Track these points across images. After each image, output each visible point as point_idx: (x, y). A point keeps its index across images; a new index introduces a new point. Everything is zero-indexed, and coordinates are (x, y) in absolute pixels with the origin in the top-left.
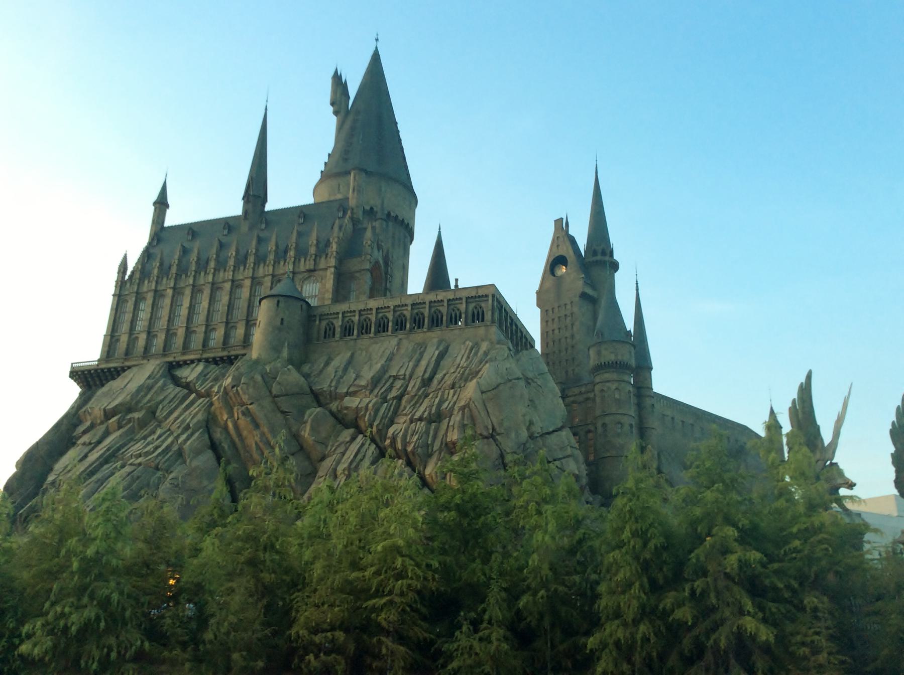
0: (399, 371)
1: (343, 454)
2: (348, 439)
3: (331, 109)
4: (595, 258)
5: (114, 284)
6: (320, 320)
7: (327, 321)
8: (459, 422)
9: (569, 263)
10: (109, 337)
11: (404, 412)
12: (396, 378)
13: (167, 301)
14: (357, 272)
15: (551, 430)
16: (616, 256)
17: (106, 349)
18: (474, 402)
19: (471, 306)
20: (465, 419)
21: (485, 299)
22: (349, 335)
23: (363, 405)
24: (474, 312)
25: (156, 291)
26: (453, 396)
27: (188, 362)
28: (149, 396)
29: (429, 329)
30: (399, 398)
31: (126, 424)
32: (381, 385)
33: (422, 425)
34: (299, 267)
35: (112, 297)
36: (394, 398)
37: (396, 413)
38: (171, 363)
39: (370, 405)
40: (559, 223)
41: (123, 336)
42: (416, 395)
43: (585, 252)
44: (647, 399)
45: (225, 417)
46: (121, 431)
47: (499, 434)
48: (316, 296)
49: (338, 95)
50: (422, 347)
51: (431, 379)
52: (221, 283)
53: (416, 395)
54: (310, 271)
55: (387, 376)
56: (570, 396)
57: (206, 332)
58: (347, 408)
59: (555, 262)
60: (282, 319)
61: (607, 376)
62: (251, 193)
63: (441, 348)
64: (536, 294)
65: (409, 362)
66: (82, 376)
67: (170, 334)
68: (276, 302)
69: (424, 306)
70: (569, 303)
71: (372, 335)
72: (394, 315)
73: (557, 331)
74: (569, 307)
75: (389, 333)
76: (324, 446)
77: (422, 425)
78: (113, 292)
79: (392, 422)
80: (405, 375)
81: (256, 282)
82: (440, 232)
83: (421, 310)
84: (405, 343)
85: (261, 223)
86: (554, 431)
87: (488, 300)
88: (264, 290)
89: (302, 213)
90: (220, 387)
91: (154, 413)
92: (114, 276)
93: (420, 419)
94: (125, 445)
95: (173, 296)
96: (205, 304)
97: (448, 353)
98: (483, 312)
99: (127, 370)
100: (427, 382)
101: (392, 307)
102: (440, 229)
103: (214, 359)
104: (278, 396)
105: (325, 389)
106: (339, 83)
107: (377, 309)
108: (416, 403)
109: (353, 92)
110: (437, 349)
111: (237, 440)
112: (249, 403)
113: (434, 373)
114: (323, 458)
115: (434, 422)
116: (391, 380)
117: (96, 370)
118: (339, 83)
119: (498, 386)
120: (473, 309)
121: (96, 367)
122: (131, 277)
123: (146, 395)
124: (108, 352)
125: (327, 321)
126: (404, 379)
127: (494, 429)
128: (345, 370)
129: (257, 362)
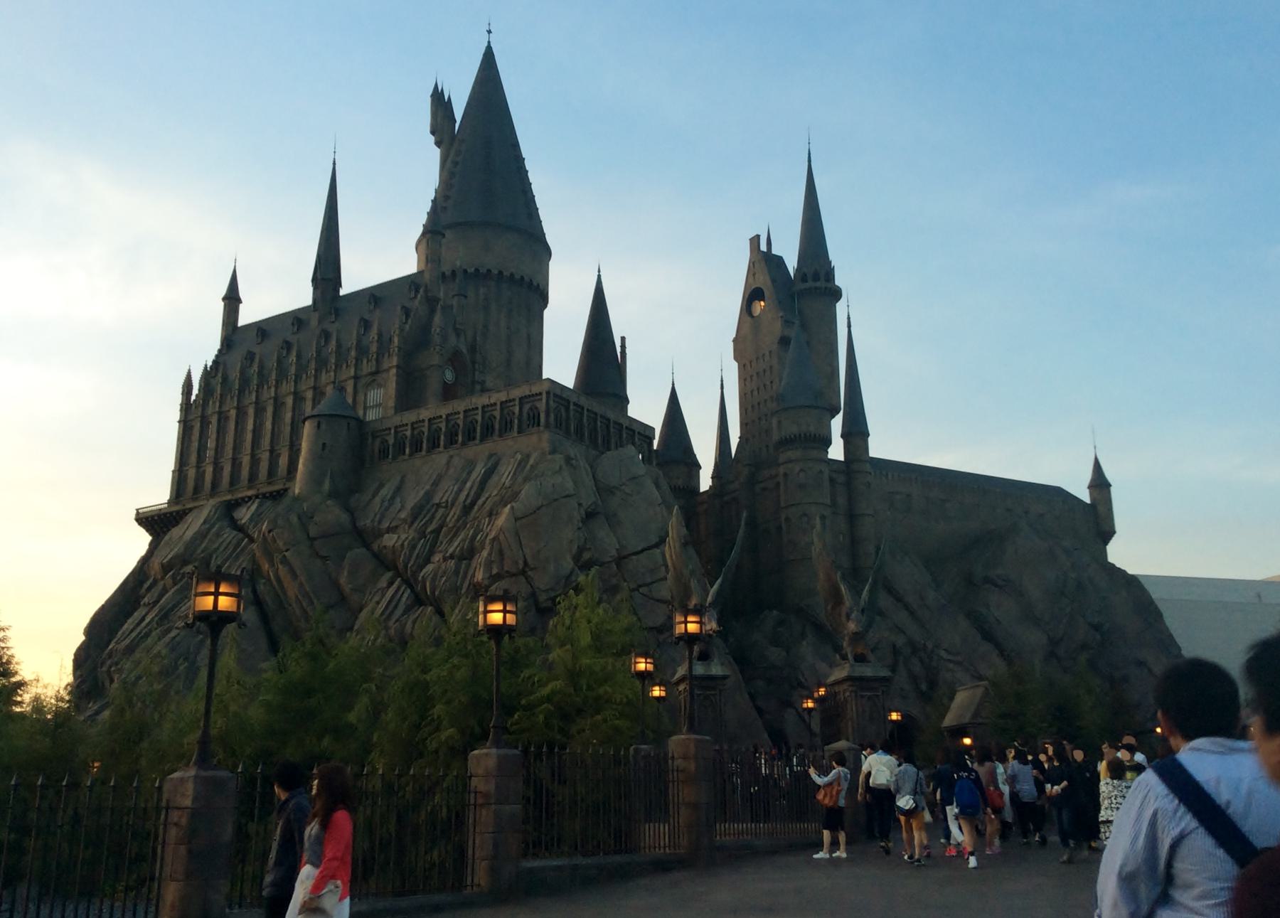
0: (442, 498)
1: (378, 603)
3: (432, 139)
4: (818, 284)
5: (179, 407)
8: (487, 558)
9: (766, 298)
11: (440, 549)
12: (438, 505)
15: (640, 549)
16: (839, 281)
17: (175, 488)
18: (504, 533)
19: (527, 407)
20: (493, 555)
21: (539, 397)
25: (220, 413)
27: (246, 499)
28: (203, 545)
29: (482, 440)
30: (437, 531)
31: (181, 580)
32: (422, 516)
33: (452, 563)
34: (362, 370)
35: (178, 424)
36: (432, 532)
37: (431, 552)
38: (229, 501)
39: (406, 543)
40: (755, 241)
41: (190, 470)
43: (795, 275)
45: (267, 566)
46: (176, 588)
47: (532, 569)
48: (380, 404)
49: (439, 119)
50: (471, 465)
51: (473, 503)
55: (431, 504)
58: (385, 547)
59: (752, 295)
61: (791, 454)
62: (319, 277)
65: (454, 485)
67: (255, 461)
68: (316, 424)
69: (476, 412)
71: (424, 453)
72: (447, 426)
73: (755, 393)
74: (767, 358)
75: (441, 449)
78: (178, 418)
79: (428, 561)
80: (447, 501)
81: (299, 399)
83: (511, 408)
84: (456, 461)
85: (331, 314)
86: (642, 551)
87: (541, 399)
90: (260, 532)
92: (178, 399)
93: (452, 557)
94: (179, 603)
95: (237, 416)
99: (188, 513)
100: (467, 509)
101: (444, 416)
102: (599, 271)
103: (271, 493)
104: (315, 539)
105: (368, 525)
107: (430, 420)
109: (459, 115)
110: (485, 465)
111: (279, 592)
112: (284, 549)
113: (478, 496)
114: (361, 610)
115: (465, 559)
118: (440, 102)
119: (538, 509)
121: (166, 511)
123: (202, 542)
126: (446, 507)
127: (526, 563)
128: (393, 498)
129: (297, 499)
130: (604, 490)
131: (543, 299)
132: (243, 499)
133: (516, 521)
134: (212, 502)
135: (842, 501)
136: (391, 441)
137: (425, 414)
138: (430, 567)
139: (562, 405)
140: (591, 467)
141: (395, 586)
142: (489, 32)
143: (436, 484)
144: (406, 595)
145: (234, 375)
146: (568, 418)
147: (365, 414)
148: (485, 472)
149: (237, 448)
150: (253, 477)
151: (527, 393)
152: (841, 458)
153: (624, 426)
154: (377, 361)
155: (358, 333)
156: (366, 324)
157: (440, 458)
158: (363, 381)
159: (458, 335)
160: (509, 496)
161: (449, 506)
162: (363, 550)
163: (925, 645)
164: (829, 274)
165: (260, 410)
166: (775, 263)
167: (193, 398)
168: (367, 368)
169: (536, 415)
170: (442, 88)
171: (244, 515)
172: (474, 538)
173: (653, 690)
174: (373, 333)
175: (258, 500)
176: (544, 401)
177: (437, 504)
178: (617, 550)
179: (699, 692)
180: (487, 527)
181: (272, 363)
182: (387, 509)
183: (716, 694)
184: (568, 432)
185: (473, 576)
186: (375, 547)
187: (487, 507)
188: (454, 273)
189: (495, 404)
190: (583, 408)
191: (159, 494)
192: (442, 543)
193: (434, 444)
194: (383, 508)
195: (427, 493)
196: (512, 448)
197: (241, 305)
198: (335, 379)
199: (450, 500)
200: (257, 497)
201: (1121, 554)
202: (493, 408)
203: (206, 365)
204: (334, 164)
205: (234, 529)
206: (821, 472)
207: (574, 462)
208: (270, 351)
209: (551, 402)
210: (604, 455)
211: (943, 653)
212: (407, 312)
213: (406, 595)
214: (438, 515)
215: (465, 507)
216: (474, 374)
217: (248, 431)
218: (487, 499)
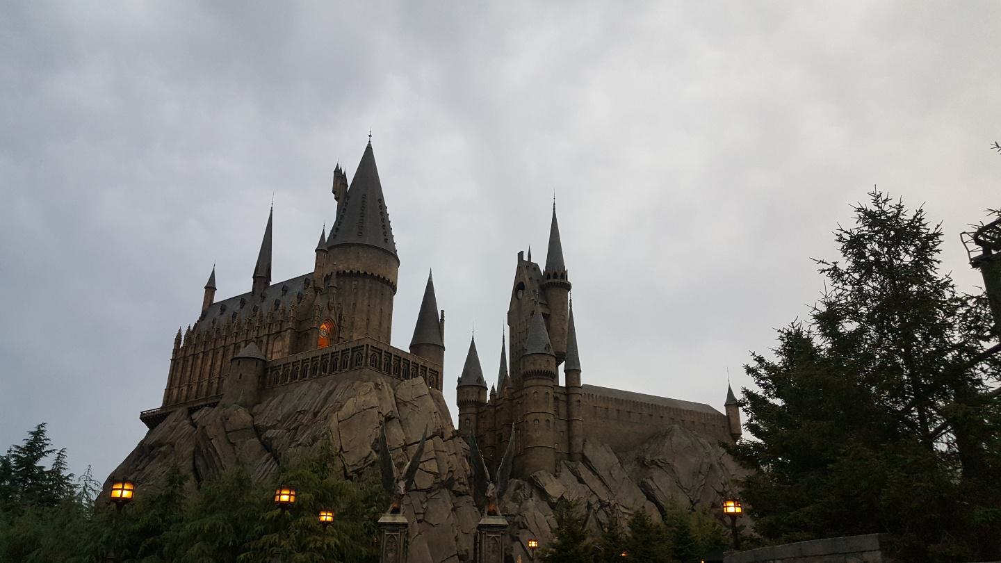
4: (556, 280)
6: (272, 372)
7: (357, 352)
10: (167, 391)
12: (300, 412)
17: (166, 399)
19: (356, 354)
38: (191, 408)
40: (521, 255)
44: (573, 396)
47: (344, 452)
51: (318, 412)
54: (277, 333)
57: (218, 383)
59: (519, 287)
60: (241, 375)
63: (331, 388)
67: (210, 383)
82: (430, 274)
89: (242, 300)
96: (219, 363)
101: (330, 353)
106: (339, 175)
109: (349, 183)
118: (339, 175)
119: (353, 415)
127: (341, 449)
130: (400, 403)
131: (394, 289)
133: (339, 422)
135: (563, 411)
140: (394, 390)
142: (370, 136)
144: (275, 467)
146: (380, 361)
159: (330, 310)
163: (609, 503)
164: (564, 275)
167: (181, 346)
168: (275, 329)
173: (726, 507)
176: (365, 350)
178: (404, 440)
184: (380, 369)
191: (155, 402)
200: (206, 406)
204: (272, 210)
207: (380, 387)
209: (369, 351)
211: (622, 509)
213: (275, 467)
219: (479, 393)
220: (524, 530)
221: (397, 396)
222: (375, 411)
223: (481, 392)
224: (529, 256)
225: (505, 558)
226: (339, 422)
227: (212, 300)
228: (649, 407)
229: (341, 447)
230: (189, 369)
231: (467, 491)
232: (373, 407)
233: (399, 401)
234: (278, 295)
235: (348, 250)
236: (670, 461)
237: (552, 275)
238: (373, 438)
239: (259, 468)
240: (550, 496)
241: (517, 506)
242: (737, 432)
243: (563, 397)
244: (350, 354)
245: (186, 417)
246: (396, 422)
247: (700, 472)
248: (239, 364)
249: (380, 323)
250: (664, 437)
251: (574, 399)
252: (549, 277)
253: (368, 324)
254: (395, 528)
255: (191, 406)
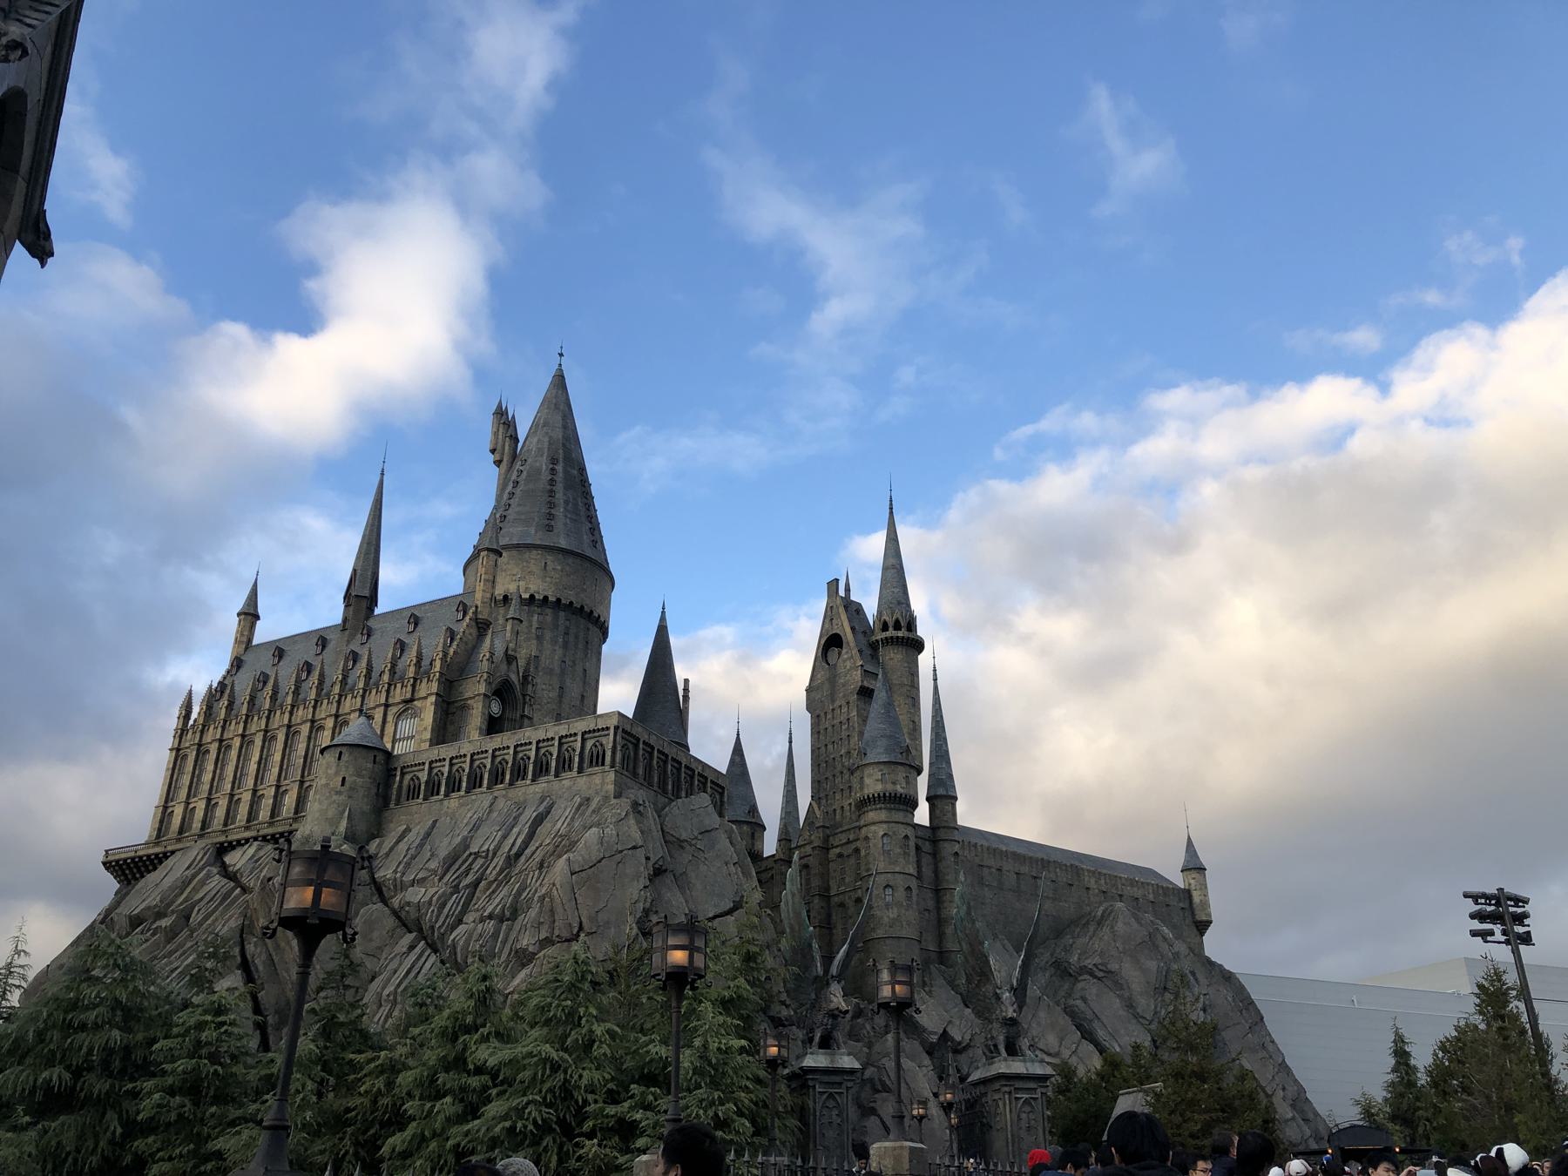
0: (481, 847)
2: (405, 950)
4: (900, 634)
6: (403, 774)
7: (412, 775)
11: (477, 906)
12: (477, 854)
13: (234, 753)
14: (471, 698)
19: (589, 744)
21: (606, 732)
22: (597, 765)
23: (426, 899)
24: (410, 787)
26: (536, 881)
27: (243, 842)
30: (476, 884)
33: (490, 925)
36: (467, 886)
38: (222, 844)
39: (435, 899)
40: (833, 585)
42: (495, 880)
44: (946, 845)
48: (413, 737)
50: (521, 806)
51: (518, 855)
52: (298, 724)
53: (495, 880)
54: (406, 702)
56: (837, 846)
57: (275, 797)
58: (408, 904)
59: (830, 643)
60: (344, 779)
63: (541, 809)
64: (805, 693)
66: (117, 868)
67: (256, 797)
69: (528, 747)
70: (844, 703)
72: (493, 762)
76: (376, 959)
77: (491, 924)
79: (460, 921)
80: (488, 850)
81: (316, 727)
82: (663, 613)
83: (527, 752)
84: (501, 803)
88: (325, 739)
91: (188, 918)
93: (490, 917)
96: (277, 757)
97: (549, 816)
98: (604, 751)
101: (491, 751)
103: (273, 836)
106: (504, 421)
108: (493, 892)
113: (526, 844)
116: (473, 857)
117: (133, 859)
118: (504, 421)
119: (600, 861)
120: (591, 748)
122: (193, 726)
124: (160, 830)
125: (412, 775)
128: (421, 845)
130: (673, 843)
132: (239, 841)
133: (572, 874)
134: (201, 843)
135: (927, 871)
136: (424, 776)
137: (466, 748)
138: (461, 929)
139: (630, 742)
141: (418, 950)
143: (476, 827)
145: (243, 695)
147: (393, 747)
148: (537, 816)
149: (237, 781)
150: (252, 815)
151: (592, 727)
152: (927, 823)
153: (696, 773)
154: (414, 686)
155: (393, 655)
156: (402, 646)
157: (482, 798)
158: (393, 711)
160: (565, 844)
161: (489, 856)
162: (380, 905)
165: (268, 738)
166: (855, 610)
168: (399, 694)
169: (601, 753)
170: (513, 415)
171: (235, 859)
172: (519, 893)
174: (411, 654)
175: (256, 843)
177: (475, 853)
179: (821, 1090)
180: (536, 881)
181: (287, 685)
182: (414, 857)
183: (842, 1093)
184: (635, 774)
185: (517, 940)
186: (396, 902)
187: (538, 857)
188: (506, 598)
189: (553, 739)
190: (638, 740)
192: (479, 899)
193: (475, 782)
194: (409, 856)
195: (465, 839)
196: (573, 785)
197: (258, 622)
198: (362, 705)
199: (490, 849)
200: (255, 839)
201: (1214, 945)
202: (550, 743)
203: (211, 686)
205: (225, 877)
206: (906, 837)
208: (287, 674)
210: (674, 803)
212: (452, 634)
214: (476, 866)
215: (508, 857)
216: (524, 708)
217: (252, 763)
218: (537, 848)
219: (753, 834)
220: (885, 1094)
221: (665, 828)
222: (640, 853)
223: (756, 835)
224: (848, 590)
225: (853, 1145)
226: (572, 874)
227: (250, 640)
228: (1066, 870)
229: (581, 923)
230: (210, 767)
231: (790, 1016)
232: (634, 848)
233: (671, 839)
234: (400, 629)
235: (527, 554)
236: (1114, 966)
237: (891, 624)
238: (641, 906)
239: (396, 961)
240: (925, 1030)
241: (865, 1049)
242: (1204, 918)
243: (927, 847)
244: (579, 744)
245: (212, 860)
246: (668, 878)
247: (1165, 988)
248: (339, 759)
249: (583, 696)
250: (1100, 923)
251: (948, 849)
252: (885, 627)
253: (561, 696)
254: (837, 1079)
255: (222, 839)
